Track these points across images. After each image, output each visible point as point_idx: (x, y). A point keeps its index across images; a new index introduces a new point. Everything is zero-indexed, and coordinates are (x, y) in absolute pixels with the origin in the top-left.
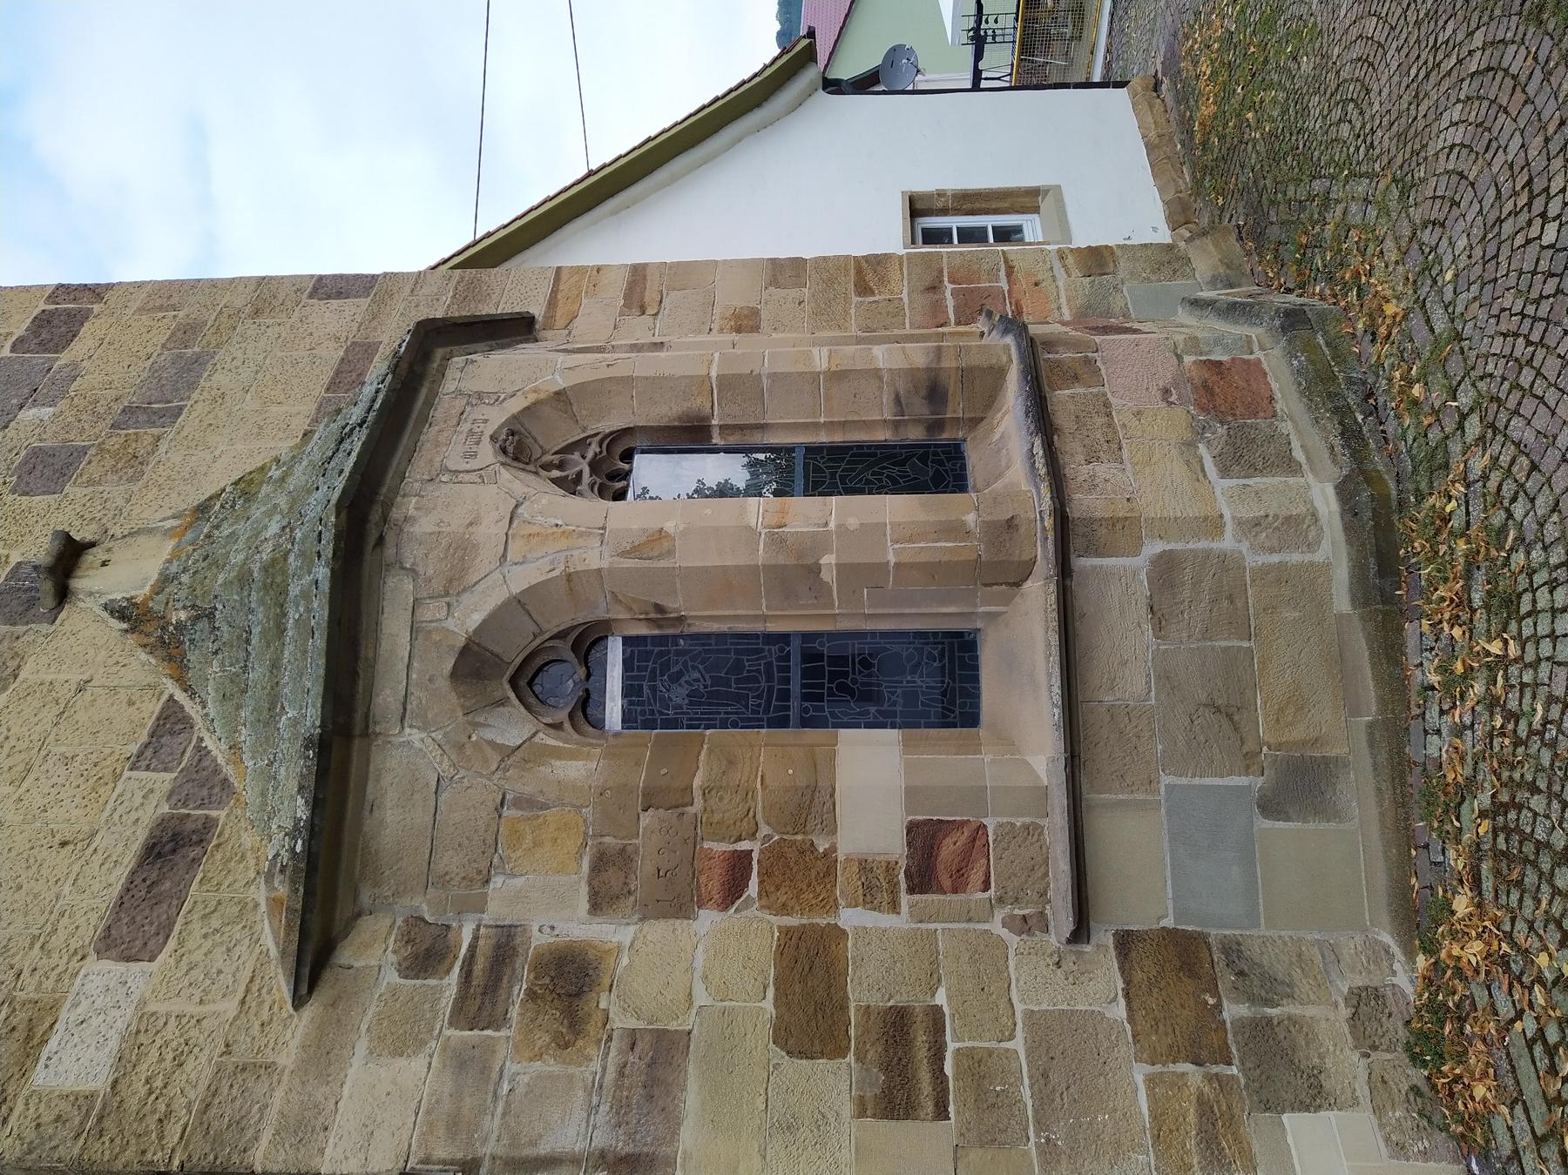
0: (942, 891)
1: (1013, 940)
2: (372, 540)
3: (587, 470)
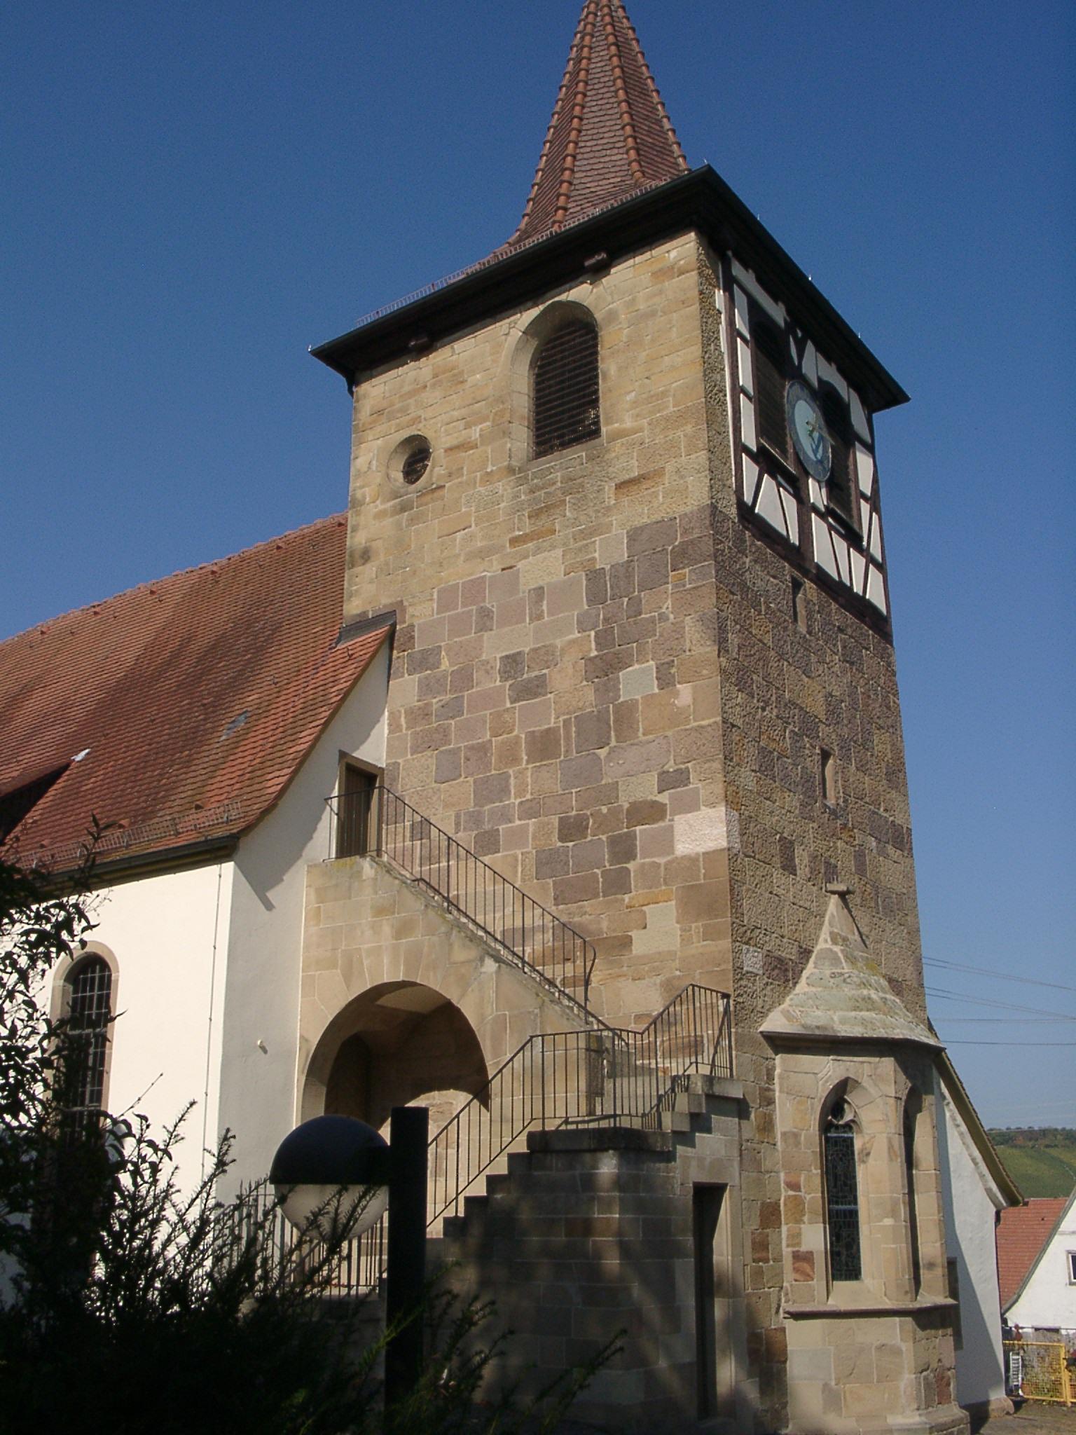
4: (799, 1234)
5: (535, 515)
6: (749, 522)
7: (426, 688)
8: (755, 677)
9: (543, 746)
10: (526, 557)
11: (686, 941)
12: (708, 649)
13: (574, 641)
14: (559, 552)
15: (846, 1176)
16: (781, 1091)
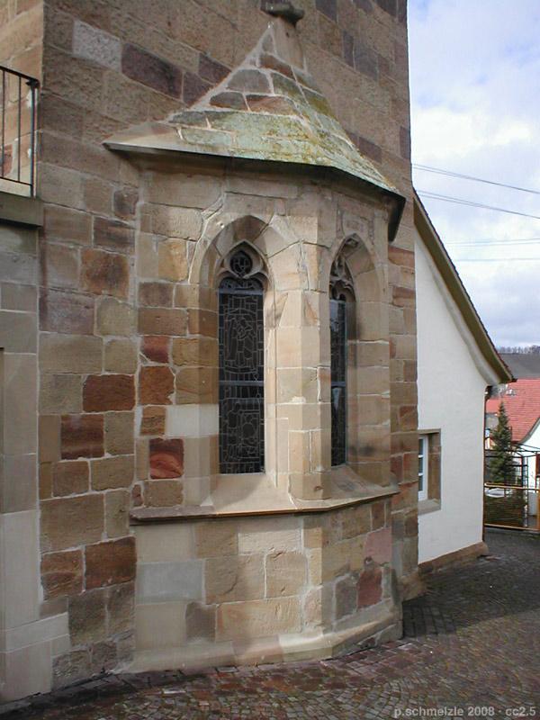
0: (151, 455)
1: (129, 490)
2: (314, 181)
3: (338, 279)
15: (248, 344)
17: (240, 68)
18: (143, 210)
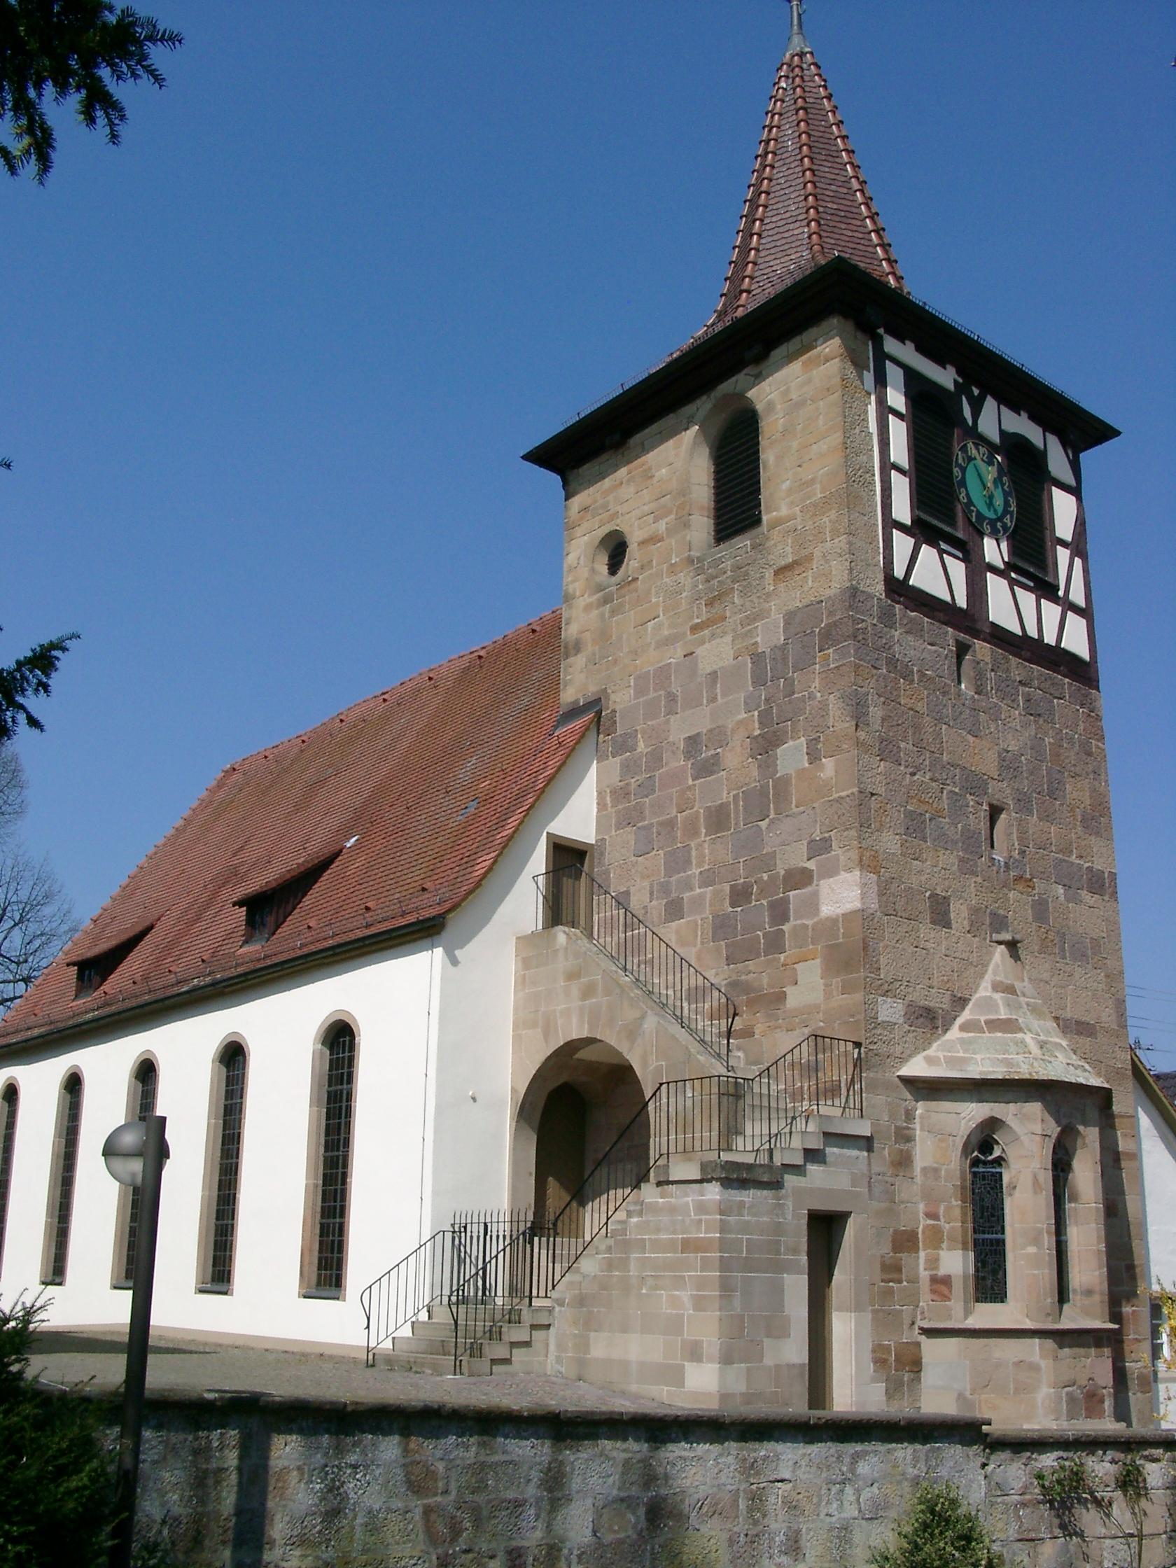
4: (937, 1260)
5: (710, 603)
6: (900, 596)
7: (627, 769)
8: (902, 745)
9: (718, 819)
10: (704, 643)
11: (828, 995)
12: (847, 725)
13: (741, 722)
14: (729, 638)
15: (993, 1208)
16: (922, 1130)
17: (977, 996)
18: (921, 1117)
